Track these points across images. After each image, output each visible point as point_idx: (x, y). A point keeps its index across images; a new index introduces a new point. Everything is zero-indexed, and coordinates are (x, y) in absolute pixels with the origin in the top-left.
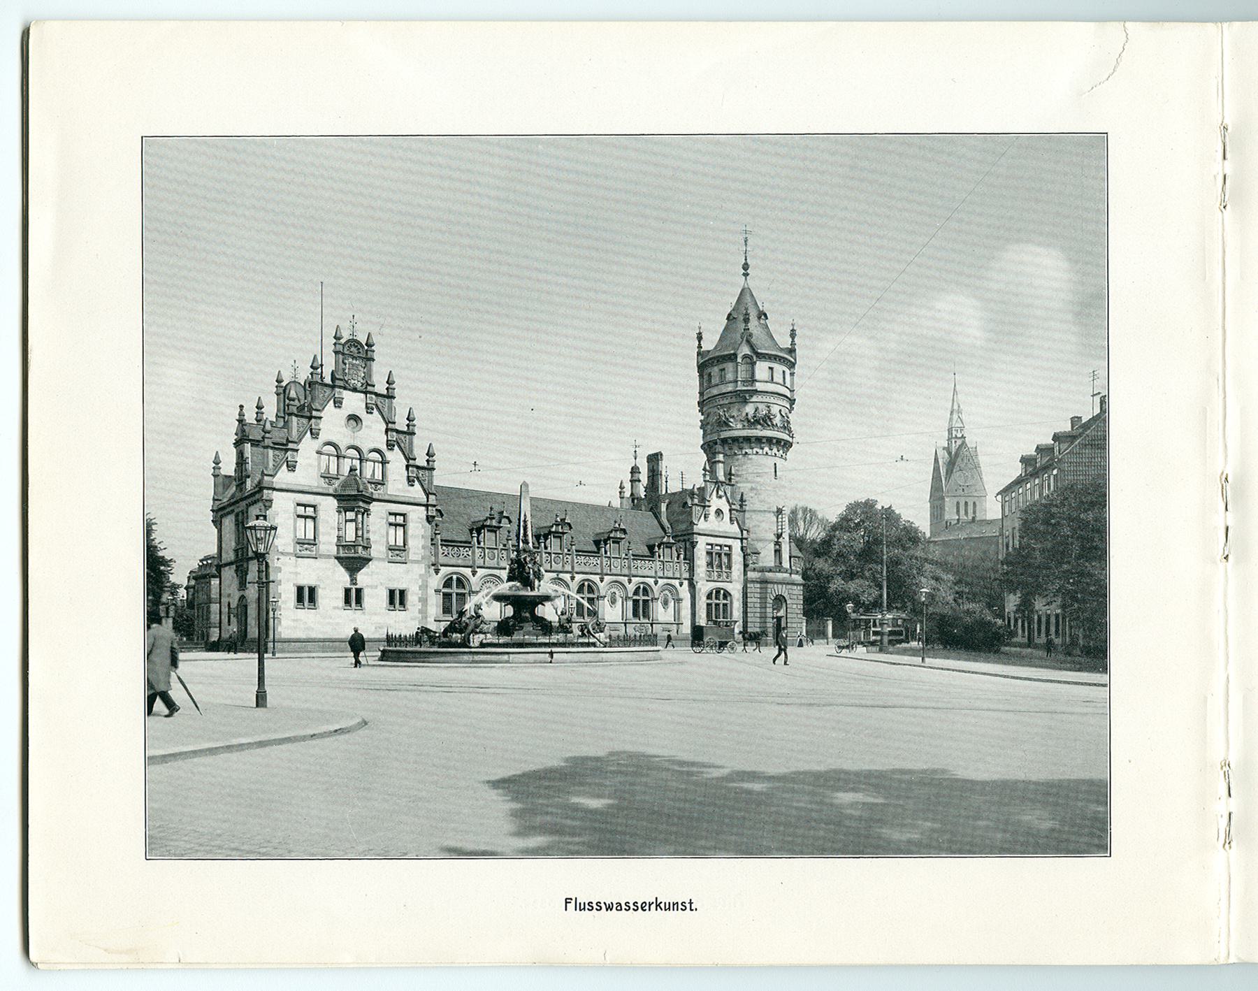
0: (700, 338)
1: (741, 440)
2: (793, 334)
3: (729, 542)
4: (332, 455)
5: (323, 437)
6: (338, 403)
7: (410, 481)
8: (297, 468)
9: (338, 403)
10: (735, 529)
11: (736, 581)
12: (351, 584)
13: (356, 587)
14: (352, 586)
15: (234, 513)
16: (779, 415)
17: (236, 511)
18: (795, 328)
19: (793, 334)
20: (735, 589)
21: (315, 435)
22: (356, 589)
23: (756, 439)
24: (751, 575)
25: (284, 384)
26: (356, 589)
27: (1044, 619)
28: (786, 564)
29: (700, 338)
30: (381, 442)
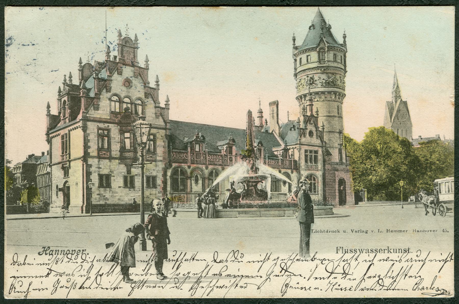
0: (294, 40)
1: (320, 93)
2: (345, 37)
3: (316, 148)
4: (129, 103)
5: (113, 91)
6: (120, 73)
7: (157, 117)
8: (346, 89)
9: (120, 73)
10: (318, 142)
11: (320, 170)
12: (127, 174)
13: (130, 175)
14: (128, 175)
15: (60, 136)
16: (339, 80)
17: (62, 134)
18: (295, 36)
19: (345, 37)
20: (319, 174)
21: (108, 90)
22: (130, 177)
23: (321, 93)
24: (327, 167)
25: (83, 65)
26: (130, 177)
27: (450, 191)
28: (344, 161)
29: (294, 40)
30: (142, 95)
